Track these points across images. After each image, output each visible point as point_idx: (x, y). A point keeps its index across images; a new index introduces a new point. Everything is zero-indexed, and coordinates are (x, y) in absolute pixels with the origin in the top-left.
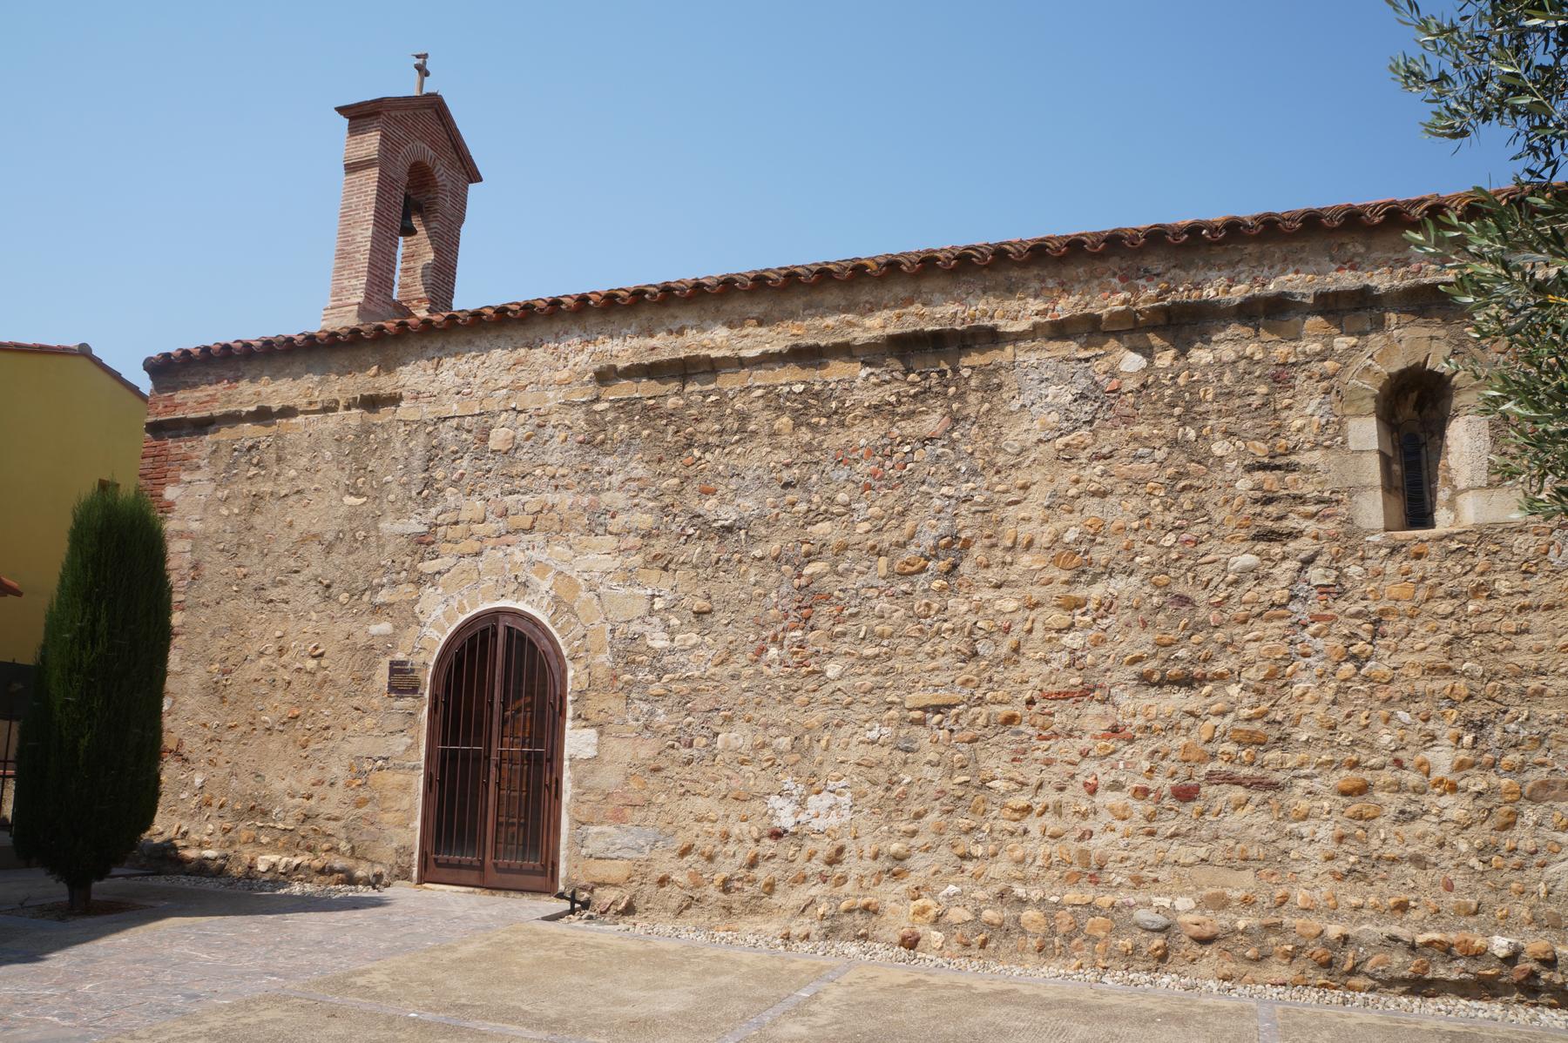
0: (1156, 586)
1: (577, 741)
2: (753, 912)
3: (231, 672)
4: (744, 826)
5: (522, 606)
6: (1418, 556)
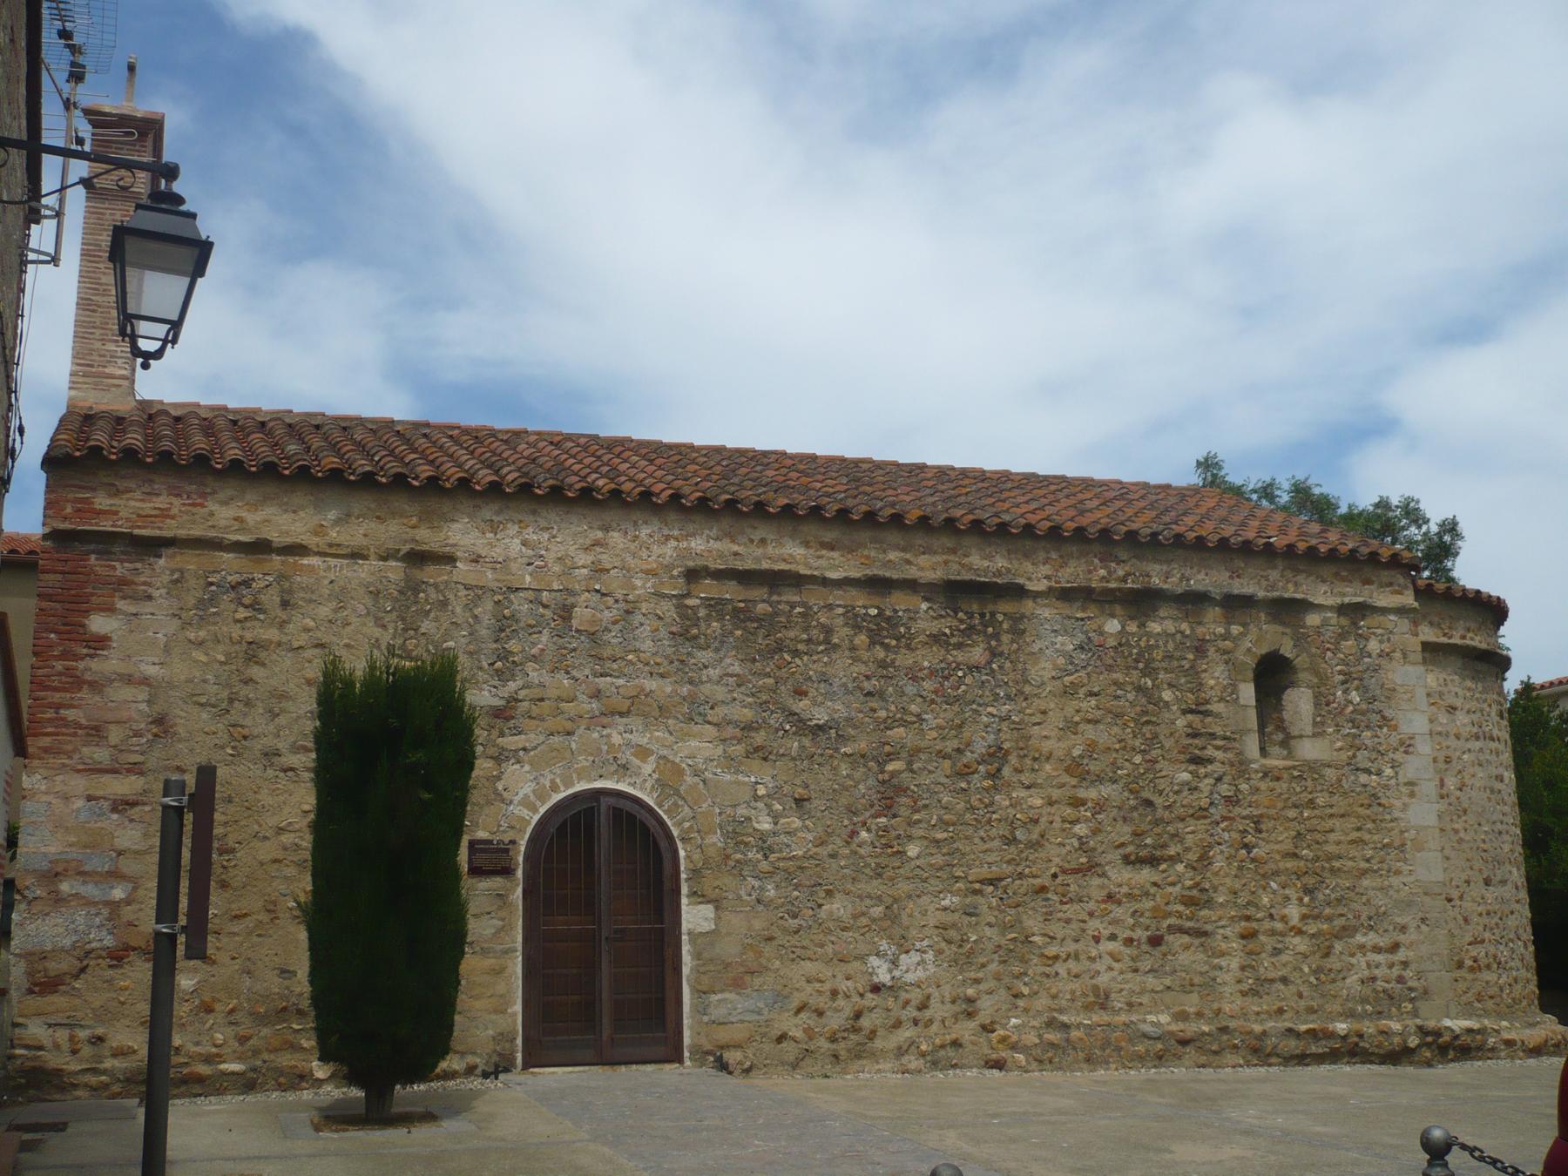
0: (1131, 791)
1: (694, 917)
2: (858, 1057)
3: (233, 851)
4: (849, 983)
5: (622, 787)
6: (1278, 779)
